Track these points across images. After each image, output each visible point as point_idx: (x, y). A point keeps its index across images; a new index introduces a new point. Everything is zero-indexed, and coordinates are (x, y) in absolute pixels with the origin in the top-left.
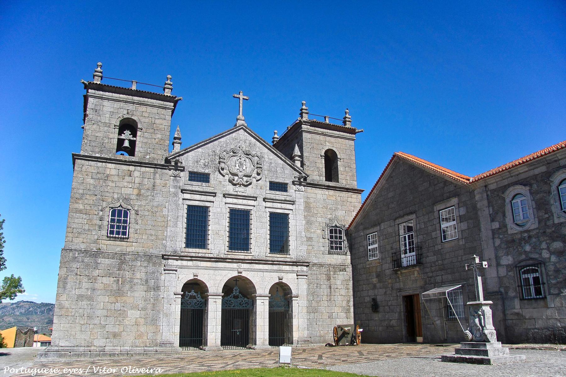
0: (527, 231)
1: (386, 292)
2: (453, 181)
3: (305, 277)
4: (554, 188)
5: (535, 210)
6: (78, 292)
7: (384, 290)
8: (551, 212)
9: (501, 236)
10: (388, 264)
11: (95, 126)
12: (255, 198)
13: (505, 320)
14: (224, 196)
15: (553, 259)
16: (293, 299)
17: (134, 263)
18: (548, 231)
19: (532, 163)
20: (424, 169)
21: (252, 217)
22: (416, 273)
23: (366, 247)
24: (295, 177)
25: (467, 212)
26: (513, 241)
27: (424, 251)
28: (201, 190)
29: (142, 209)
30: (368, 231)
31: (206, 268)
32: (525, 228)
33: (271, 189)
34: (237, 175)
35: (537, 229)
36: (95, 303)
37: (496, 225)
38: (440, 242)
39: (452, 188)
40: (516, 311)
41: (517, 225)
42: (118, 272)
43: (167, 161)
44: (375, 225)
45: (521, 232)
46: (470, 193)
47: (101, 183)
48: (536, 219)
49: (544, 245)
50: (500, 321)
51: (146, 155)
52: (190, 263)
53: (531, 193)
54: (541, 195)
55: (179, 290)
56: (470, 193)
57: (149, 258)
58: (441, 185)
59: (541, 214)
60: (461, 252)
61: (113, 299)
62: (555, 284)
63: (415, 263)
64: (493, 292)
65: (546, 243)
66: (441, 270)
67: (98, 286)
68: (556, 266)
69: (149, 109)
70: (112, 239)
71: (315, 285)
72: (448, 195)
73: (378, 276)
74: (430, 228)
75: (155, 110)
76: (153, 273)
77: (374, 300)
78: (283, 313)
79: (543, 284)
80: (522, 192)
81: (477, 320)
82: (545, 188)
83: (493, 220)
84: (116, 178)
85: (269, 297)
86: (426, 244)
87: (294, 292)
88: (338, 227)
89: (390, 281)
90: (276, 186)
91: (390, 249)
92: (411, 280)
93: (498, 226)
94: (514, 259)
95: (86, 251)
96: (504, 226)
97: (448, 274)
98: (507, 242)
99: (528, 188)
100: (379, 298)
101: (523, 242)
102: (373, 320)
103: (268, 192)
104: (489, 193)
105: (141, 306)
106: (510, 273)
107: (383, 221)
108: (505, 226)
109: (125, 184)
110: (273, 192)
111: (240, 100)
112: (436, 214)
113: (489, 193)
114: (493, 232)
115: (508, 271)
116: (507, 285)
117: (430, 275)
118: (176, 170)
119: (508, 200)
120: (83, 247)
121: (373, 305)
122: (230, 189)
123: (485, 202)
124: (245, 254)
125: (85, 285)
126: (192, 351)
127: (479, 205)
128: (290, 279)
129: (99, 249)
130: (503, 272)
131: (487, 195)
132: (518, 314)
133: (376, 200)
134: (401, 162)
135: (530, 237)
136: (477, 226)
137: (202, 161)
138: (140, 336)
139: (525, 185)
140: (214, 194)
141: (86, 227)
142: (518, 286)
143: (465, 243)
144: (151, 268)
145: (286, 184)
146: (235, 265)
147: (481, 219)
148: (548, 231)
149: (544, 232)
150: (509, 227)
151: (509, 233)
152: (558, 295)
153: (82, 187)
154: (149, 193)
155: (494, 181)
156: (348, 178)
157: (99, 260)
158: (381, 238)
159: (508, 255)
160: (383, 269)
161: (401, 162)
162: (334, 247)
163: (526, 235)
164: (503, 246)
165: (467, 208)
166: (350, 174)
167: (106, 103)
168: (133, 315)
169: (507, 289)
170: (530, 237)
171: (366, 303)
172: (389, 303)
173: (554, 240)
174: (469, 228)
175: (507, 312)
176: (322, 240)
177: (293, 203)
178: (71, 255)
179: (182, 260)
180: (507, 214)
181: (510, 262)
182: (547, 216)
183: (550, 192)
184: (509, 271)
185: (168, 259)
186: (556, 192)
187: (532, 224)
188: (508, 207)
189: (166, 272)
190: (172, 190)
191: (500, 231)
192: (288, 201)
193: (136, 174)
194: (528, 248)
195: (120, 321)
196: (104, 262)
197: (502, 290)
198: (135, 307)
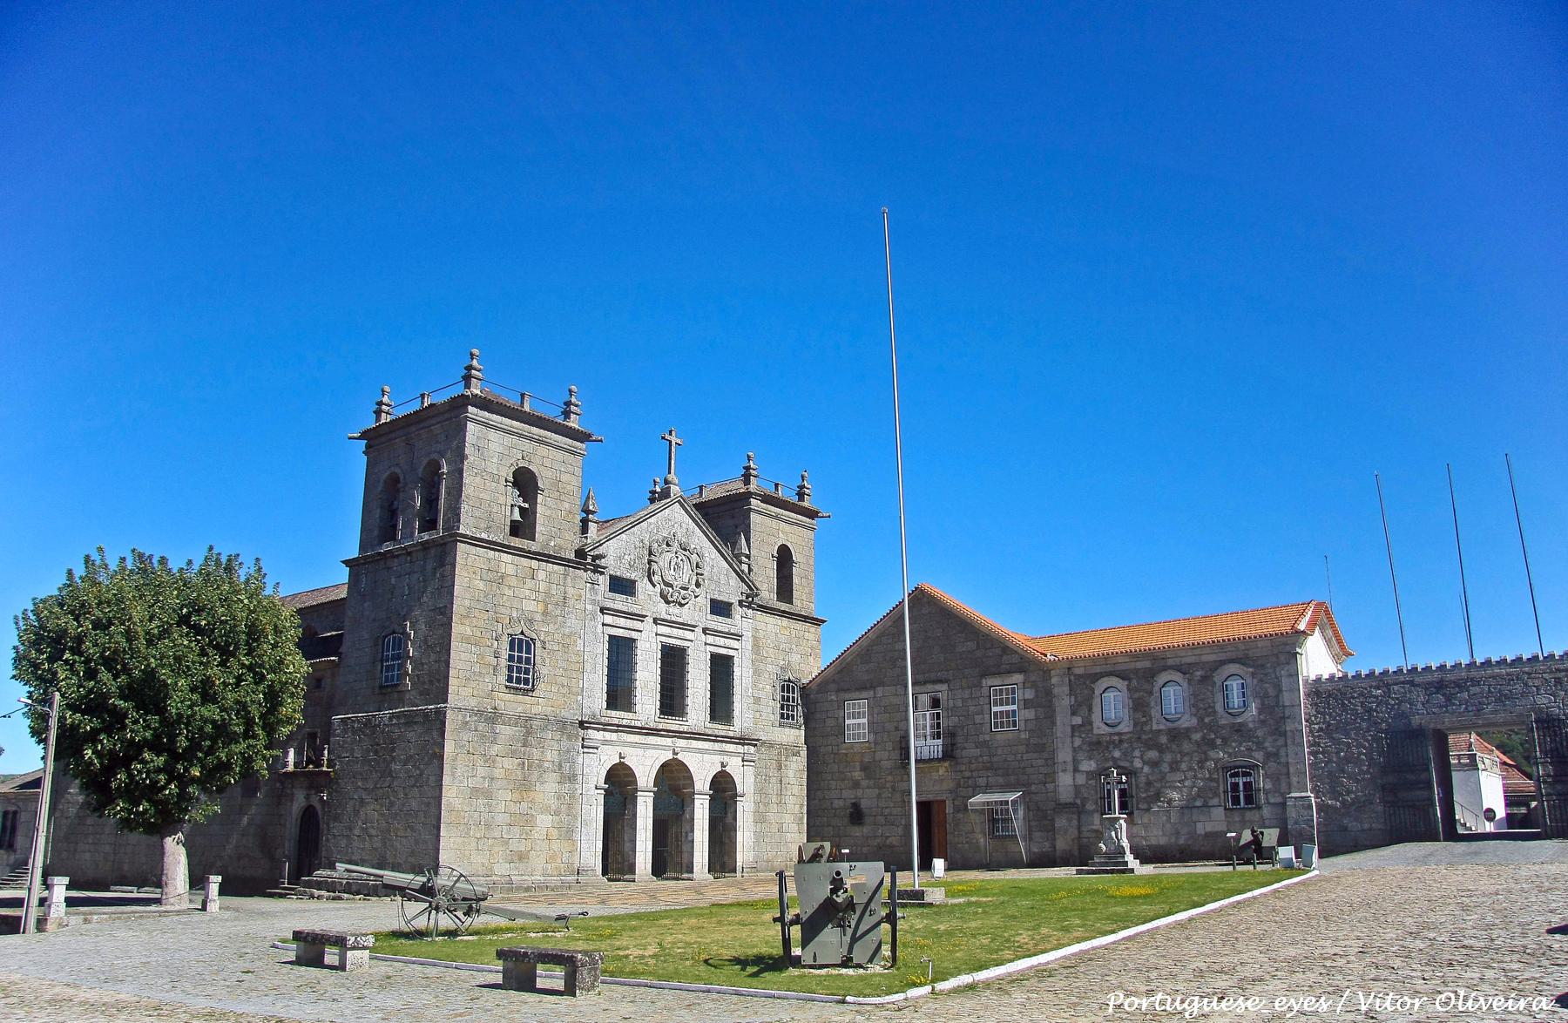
0: (1119, 734)
1: (880, 794)
2: (1020, 651)
3: (752, 764)
4: (1156, 689)
5: (1131, 710)
6: (472, 783)
7: (877, 791)
8: (1150, 716)
9: (1083, 736)
10: (887, 752)
11: (478, 479)
12: (690, 627)
13: (1079, 838)
14: (655, 621)
15: (1146, 769)
16: (738, 798)
17: (544, 735)
18: (1144, 737)
19: (1134, 656)
20: (969, 621)
21: (690, 660)
22: (941, 772)
23: (841, 720)
24: (742, 593)
25: (1037, 696)
26: (1099, 743)
27: (959, 739)
28: (625, 609)
29: (550, 639)
30: (847, 696)
31: (700, 751)
32: (1117, 730)
33: (712, 612)
34: (671, 586)
35: (1130, 733)
36: (494, 802)
37: (1078, 720)
38: (989, 730)
39: (1015, 659)
40: (1094, 827)
41: (1106, 724)
42: (523, 749)
43: (580, 553)
44: (863, 687)
45: (1111, 734)
46: (1044, 672)
47: (494, 588)
48: (1132, 722)
49: (1137, 753)
50: (1073, 840)
51: (551, 540)
52: (614, 736)
53: (1128, 689)
54: (1141, 693)
55: (601, 783)
56: (1044, 672)
57: (562, 724)
58: (998, 651)
59: (1139, 715)
60: (1022, 748)
61: (516, 796)
62: (1144, 798)
63: (940, 756)
64: (1066, 804)
65: (1141, 751)
66: (988, 769)
67: (498, 773)
68: (1148, 778)
69: (553, 453)
70: (512, 691)
71: (764, 777)
72: (1008, 667)
73: (864, 768)
74: (972, 708)
75: (560, 455)
76: (568, 751)
77: (856, 806)
78: (10, 816)
79: (1132, 797)
80: (1119, 686)
81: (1113, 834)
82: (1146, 686)
83: (1074, 713)
84: (513, 582)
85: (654, 793)
86: (963, 730)
87: (739, 790)
88: (791, 682)
89: (890, 778)
90: (720, 608)
91: (893, 729)
92: (931, 779)
93: (1080, 723)
94: (1098, 765)
95: (480, 713)
96: (1088, 723)
97: (998, 775)
98: (1090, 744)
99: (1126, 683)
100: (864, 804)
101: (1111, 746)
102: (850, 836)
103: (709, 616)
104: (1072, 678)
105: (553, 807)
106: (1090, 782)
107: (882, 684)
108: (1091, 723)
109: (527, 592)
110: (715, 617)
111: (670, 445)
112: (985, 691)
113: (1072, 678)
114: (1073, 727)
115: (1088, 779)
116: (1086, 795)
117: (967, 774)
118: (595, 571)
119: (1097, 692)
120: (473, 703)
121: (851, 814)
122: (662, 609)
123: (1066, 689)
124: (681, 723)
125: (481, 771)
126: (728, 879)
127: (1056, 691)
128: (735, 767)
129: (495, 708)
130: (1081, 779)
131: (1070, 681)
132: (1097, 831)
133: (870, 648)
134: (925, 599)
135: (1121, 741)
136: (1051, 717)
137: (626, 557)
138: (552, 858)
139: (1123, 679)
140: (640, 617)
141: (477, 668)
142: (1101, 798)
143: (1030, 737)
144: (565, 743)
145: (730, 604)
146: (668, 741)
147: (1058, 709)
148: (1144, 737)
149: (1139, 738)
150: (1095, 725)
151: (1095, 732)
152: (1148, 810)
153: (468, 596)
154: (558, 612)
155: (1083, 665)
156: (804, 597)
157: (499, 728)
158: (876, 710)
159: (1090, 759)
160: (877, 758)
161: (925, 599)
162: (785, 717)
163: (1116, 738)
164: (1085, 747)
165: (1037, 691)
166: (807, 590)
167: (492, 434)
168: (544, 821)
169: (1084, 801)
170: (1121, 741)
171: (836, 809)
172: (886, 812)
173: (1150, 749)
174: (1037, 718)
175: (1083, 829)
176: (771, 703)
177: (737, 637)
178: (460, 717)
179: (604, 730)
180: (1094, 709)
181: (1092, 769)
182: (1144, 719)
183: (1151, 693)
184: (1090, 780)
185: (587, 728)
186: (1158, 694)
187: (1125, 727)
188: (1096, 701)
189: (586, 750)
190: (589, 607)
191: (1083, 729)
192: (732, 634)
193: (541, 575)
194: (1117, 754)
195: (527, 834)
196: (505, 731)
197: (1078, 801)
198: (546, 810)
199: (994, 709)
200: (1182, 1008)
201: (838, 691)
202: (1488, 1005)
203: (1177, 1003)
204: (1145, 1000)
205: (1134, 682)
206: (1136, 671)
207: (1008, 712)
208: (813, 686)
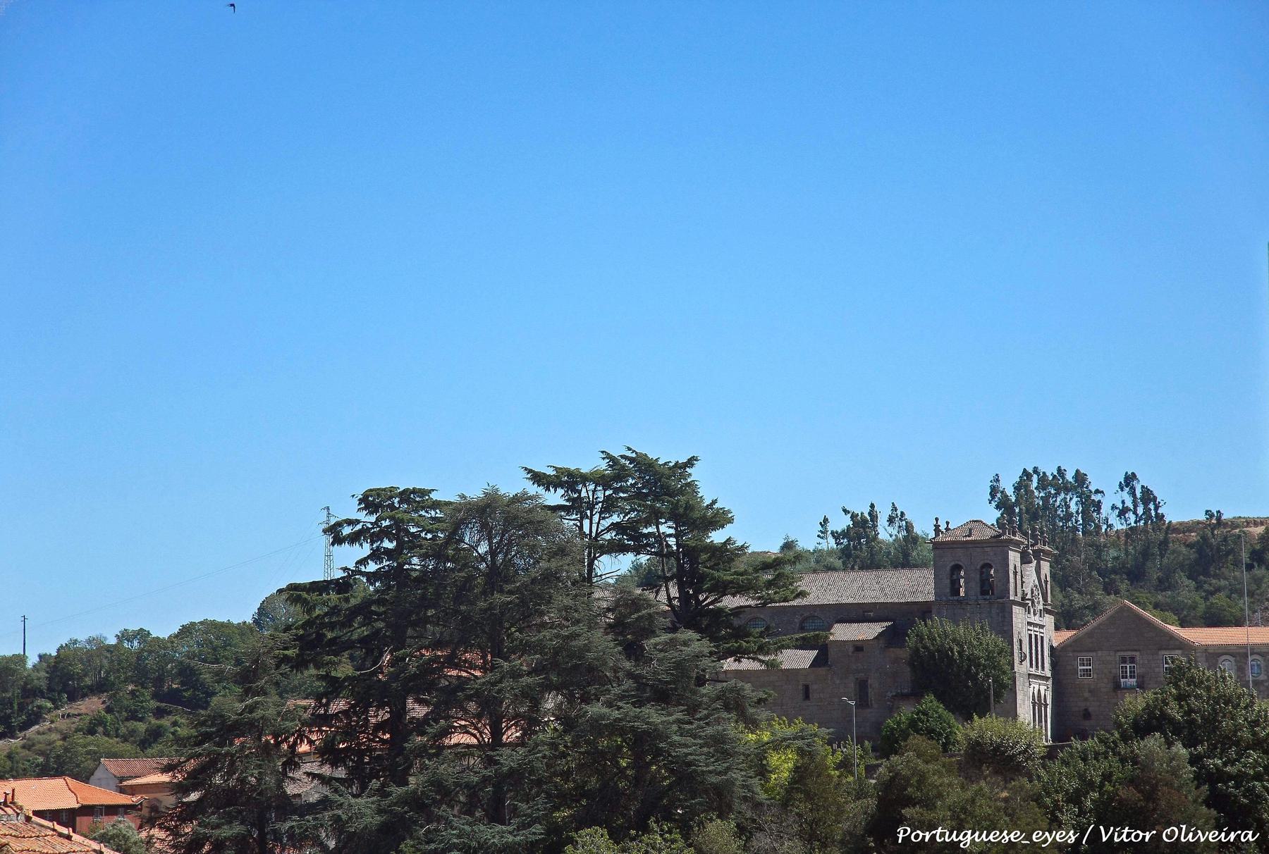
7: (1098, 703)
59: (1239, 673)
77: (1086, 710)
89: (1106, 697)
112: (1161, 657)
183: (1246, 663)
199: (1091, 667)
200: (988, 839)
201: (1074, 651)
202: (1205, 838)
203: (1124, 836)
204: (928, 833)
205: (1238, 658)
206: (1239, 654)
207: (1087, 669)
208: (1059, 648)
